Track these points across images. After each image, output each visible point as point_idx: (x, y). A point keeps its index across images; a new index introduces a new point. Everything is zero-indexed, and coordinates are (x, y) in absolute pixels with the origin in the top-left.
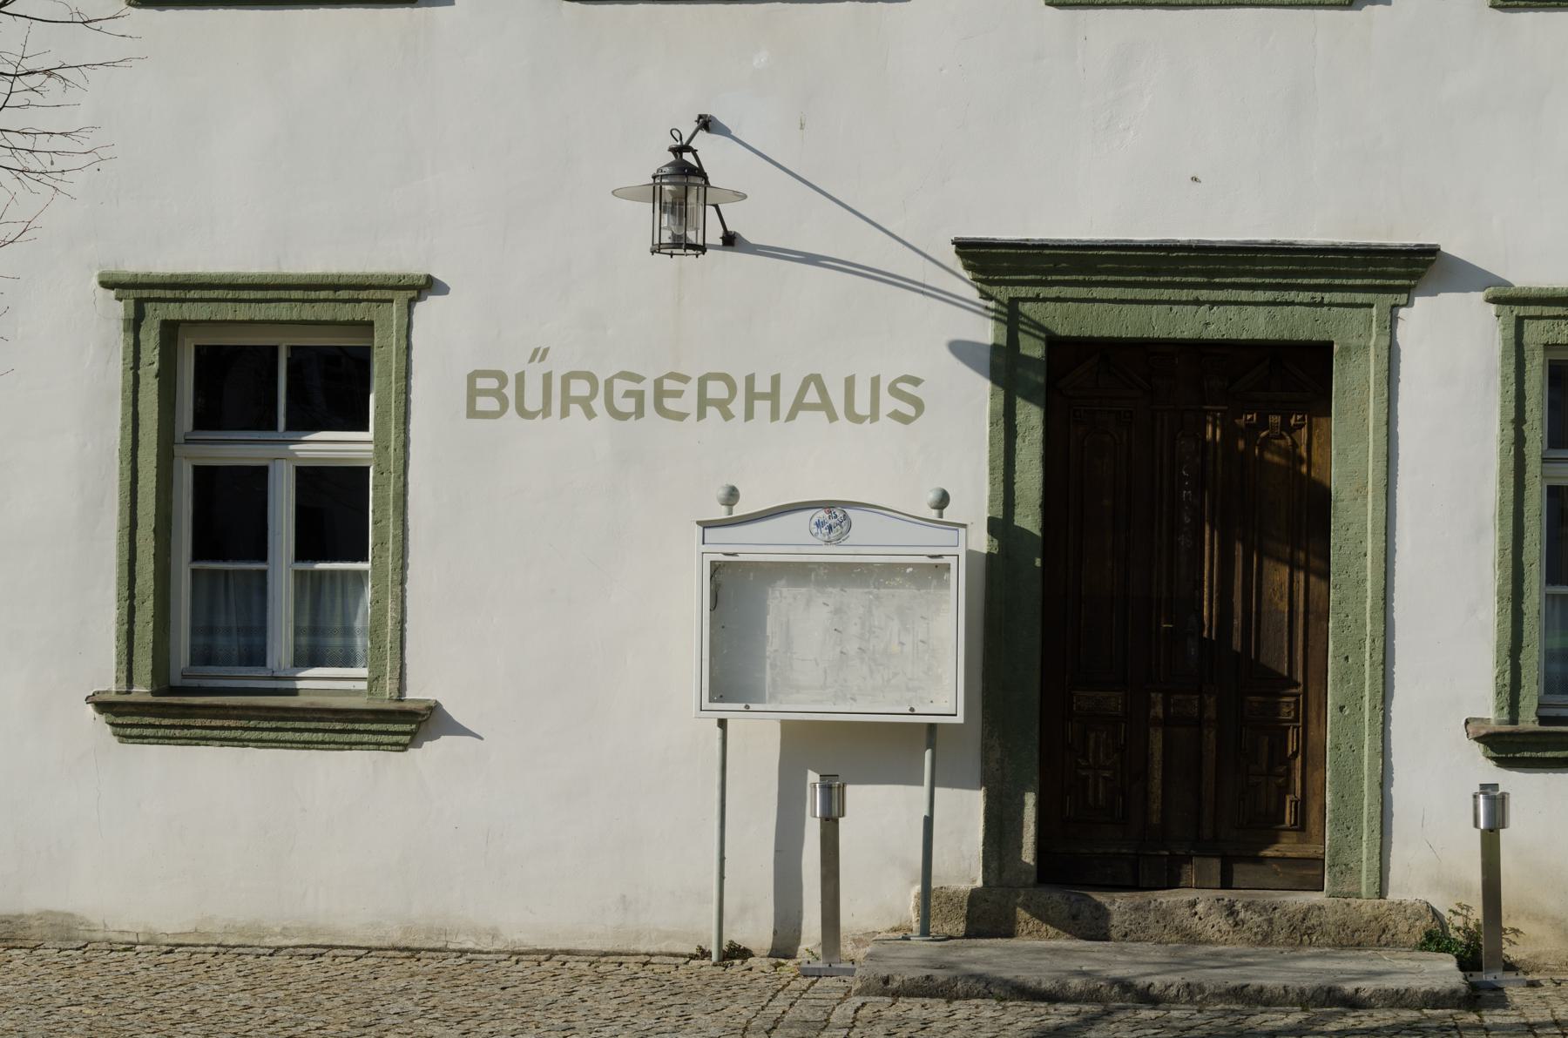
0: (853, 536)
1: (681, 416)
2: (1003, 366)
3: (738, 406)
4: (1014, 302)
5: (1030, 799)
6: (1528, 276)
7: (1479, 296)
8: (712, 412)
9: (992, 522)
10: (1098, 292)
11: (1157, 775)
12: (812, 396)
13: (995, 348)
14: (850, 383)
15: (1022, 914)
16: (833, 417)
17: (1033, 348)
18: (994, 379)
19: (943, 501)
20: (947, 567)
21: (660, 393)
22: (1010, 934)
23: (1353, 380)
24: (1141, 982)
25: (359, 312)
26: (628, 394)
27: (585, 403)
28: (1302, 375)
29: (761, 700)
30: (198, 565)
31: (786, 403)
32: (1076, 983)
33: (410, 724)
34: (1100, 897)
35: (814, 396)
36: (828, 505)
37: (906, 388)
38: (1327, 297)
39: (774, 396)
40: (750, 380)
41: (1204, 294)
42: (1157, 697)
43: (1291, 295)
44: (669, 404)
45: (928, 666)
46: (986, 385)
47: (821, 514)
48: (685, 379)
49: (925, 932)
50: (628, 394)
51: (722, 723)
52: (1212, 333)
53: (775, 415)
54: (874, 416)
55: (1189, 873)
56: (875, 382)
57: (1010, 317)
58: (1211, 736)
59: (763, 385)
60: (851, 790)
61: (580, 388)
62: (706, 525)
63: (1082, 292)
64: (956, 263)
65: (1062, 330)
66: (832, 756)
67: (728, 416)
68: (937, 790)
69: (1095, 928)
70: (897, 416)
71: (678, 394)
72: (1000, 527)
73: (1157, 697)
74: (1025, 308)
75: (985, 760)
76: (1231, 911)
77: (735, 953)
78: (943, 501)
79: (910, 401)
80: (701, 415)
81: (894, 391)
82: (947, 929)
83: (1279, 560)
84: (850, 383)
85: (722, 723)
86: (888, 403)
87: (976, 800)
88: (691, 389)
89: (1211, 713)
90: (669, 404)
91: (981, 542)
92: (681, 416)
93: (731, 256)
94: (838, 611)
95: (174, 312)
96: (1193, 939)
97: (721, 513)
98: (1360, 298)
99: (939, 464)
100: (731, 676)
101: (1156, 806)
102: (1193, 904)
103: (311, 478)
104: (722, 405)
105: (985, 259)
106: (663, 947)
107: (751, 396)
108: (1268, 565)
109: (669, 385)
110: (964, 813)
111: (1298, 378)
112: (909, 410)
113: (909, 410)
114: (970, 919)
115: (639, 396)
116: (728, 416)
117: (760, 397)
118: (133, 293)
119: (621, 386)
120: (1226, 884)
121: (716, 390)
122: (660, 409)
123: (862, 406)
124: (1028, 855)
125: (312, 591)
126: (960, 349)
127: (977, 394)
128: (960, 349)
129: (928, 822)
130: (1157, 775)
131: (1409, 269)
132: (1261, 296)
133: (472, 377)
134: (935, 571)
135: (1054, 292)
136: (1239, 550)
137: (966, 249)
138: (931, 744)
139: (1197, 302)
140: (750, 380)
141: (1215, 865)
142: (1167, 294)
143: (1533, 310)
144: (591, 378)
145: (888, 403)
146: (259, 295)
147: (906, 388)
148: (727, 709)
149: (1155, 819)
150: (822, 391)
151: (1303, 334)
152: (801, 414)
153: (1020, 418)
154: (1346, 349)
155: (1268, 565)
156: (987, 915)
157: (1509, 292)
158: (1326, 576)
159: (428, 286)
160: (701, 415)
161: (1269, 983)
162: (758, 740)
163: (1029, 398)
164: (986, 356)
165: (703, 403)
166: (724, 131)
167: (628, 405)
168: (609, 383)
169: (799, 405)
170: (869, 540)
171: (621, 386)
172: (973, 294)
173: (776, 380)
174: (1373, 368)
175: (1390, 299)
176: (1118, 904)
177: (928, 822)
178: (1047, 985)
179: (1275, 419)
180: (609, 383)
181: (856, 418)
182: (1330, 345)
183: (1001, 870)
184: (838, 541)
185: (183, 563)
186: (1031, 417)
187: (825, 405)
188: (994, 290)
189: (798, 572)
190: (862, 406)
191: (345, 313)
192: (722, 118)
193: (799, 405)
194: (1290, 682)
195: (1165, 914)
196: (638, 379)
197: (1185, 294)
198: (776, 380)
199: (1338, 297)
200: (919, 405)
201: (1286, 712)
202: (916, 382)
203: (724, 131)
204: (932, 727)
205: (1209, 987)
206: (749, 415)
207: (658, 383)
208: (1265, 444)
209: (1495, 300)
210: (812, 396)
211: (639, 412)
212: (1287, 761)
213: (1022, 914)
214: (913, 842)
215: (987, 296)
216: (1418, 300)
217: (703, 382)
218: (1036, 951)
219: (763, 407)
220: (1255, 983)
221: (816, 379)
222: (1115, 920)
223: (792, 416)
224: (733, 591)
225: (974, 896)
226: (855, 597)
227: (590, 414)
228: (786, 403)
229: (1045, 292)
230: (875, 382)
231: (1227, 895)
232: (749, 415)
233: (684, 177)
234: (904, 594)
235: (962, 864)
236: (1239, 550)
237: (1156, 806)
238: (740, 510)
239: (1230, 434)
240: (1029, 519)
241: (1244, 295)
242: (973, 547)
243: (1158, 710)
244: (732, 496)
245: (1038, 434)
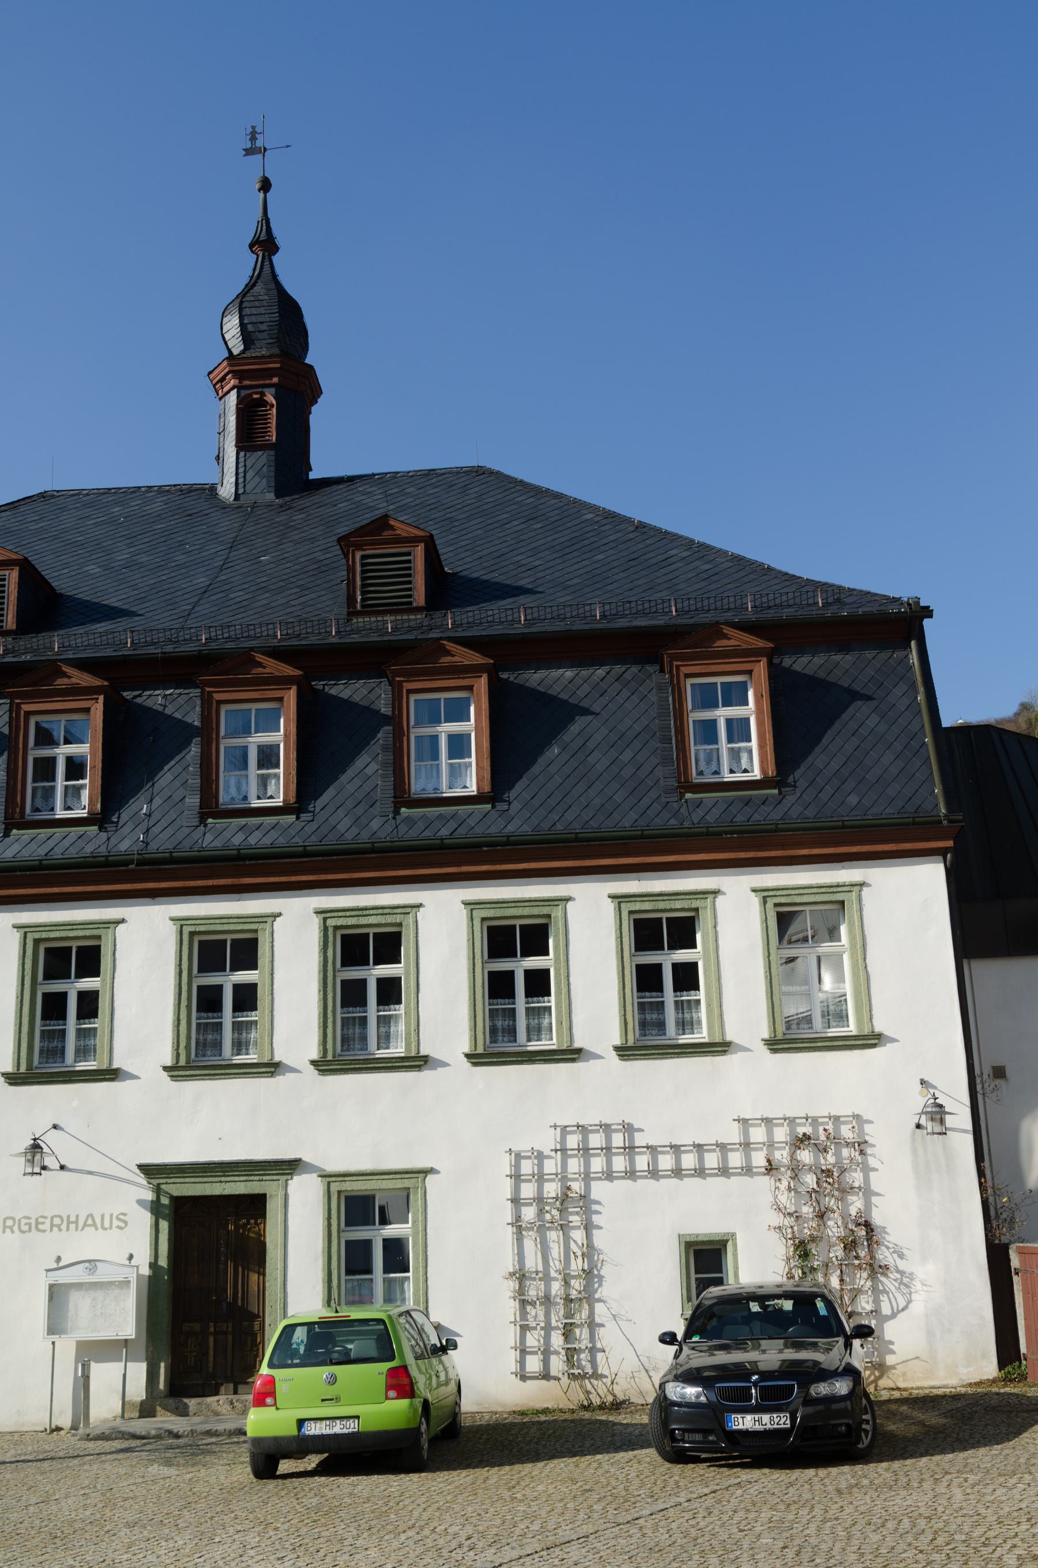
0: (98, 1272)
1: (44, 1231)
2: (155, 1208)
3: (64, 1227)
4: (159, 1184)
5: (162, 1365)
6: (331, 1167)
7: (315, 1175)
8: (55, 1229)
9: (150, 1264)
10: (187, 1180)
11: (211, 1353)
12: (90, 1222)
13: (152, 1201)
14: (103, 1216)
15: (159, 1408)
16: (97, 1229)
17: (165, 1201)
18: (152, 1213)
19: (131, 1257)
20: (129, 1282)
21: (37, 1223)
22: (154, 1416)
23: (273, 1207)
24: (175, 1431)
25: (398, 919)
26: (26, 1224)
27: (59, 1226)
28: (256, 1204)
29: (66, 1333)
30: (386, 1276)
31: (81, 1224)
32: (153, 1432)
33: (111, 1074)
34: (186, 1400)
35: (90, 1223)
36: (89, 1261)
37: (122, 1217)
38: (264, 1178)
39: (76, 1222)
40: (68, 1217)
41: (223, 1179)
42: (211, 1324)
43: (252, 1178)
44: (40, 1227)
45: (123, 1317)
46: (149, 1214)
47: (87, 1264)
48: (46, 1218)
49: (123, 1417)
50: (26, 1224)
51: (53, 1343)
52: (226, 1192)
53: (77, 1229)
54: (111, 1228)
55: (223, 1389)
56: (111, 1215)
57: (158, 1190)
58: (230, 1337)
59: (73, 1219)
60: (93, 1364)
61: (9, 1223)
62: (48, 1271)
63: (182, 1180)
64: (138, 1171)
65: (175, 1194)
66: (91, 1352)
67: (60, 1230)
68: (128, 1364)
69: (183, 1412)
70: (119, 1227)
71: (43, 1223)
72: (154, 1265)
73: (211, 1324)
74: (163, 1187)
75: (147, 1351)
76: (232, 1403)
77: (58, 1429)
78: (131, 1257)
79: (123, 1221)
80: (51, 1230)
81: (118, 1218)
82: (132, 1416)
83: (254, 1272)
84: (103, 1216)
85: (53, 1343)
86: (116, 1223)
87: (143, 1367)
88: (48, 1221)
89: (230, 1329)
90: (40, 1227)
91: (146, 1271)
92: (44, 1231)
93: (62, 1173)
94: (94, 1299)
95: (37, 936)
96: (217, 1414)
97: (55, 1266)
98: (275, 1177)
99: (129, 1244)
100: (55, 1326)
101: (211, 1365)
102: (218, 1401)
103: (529, 974)
104: (59, 1226)
105: (148, 1170)
106: (32, 1429)
107: (69, 1223)
108: (251, 1273)
109: (40, 1220)
110: (138, 1371)
111: (255, 1206)
112: (123, 1225)
113: (123, 1225)
114: (141, 1411)
115: (30, 1225)
116: (60, 1230)
117: (71, 1223)
118: (179, 923)
119: (24, 1221)
120: (235, 1392)
121: (57, 1221)
122: (37, 1229)
123: (107, 1224)
124: (162, 1386)
125: (389, 1284)
126: (141, 1202)
127: (146, 1218)
128: (141, 1202)
129: (125, 1376)
130: (211, 1353)
131: (291, 1167)
132: (242, 1178)
133: (5, 1220)
134: (126, 1283)
135: (172, 1180)
136: (240, 1269)
137: (142, 1167)
138: (126, 1347)
139: (221, 1182)
140: (68, 1217)
141: (231, 1386)
142: (210, 1179)
143: (329, 915)
144: (13, 1219)
145: (116, 1223)
146: (360, 913)
147: (122, 1217)
148: (54, 1338)
149: (211, 1370)
150: (93, 1219)
151: (256, 1192)
152: (86, 1228)
153: (160, 1226)
154: (271, 1196)
155: (251, 1273)
156: (146, 1410)
157: (324, 1173)
158: (264, 1275)
159: (280, 915)
160: (51, 1230)
161: (219, 1428)
162: (67, 1347)
163: (163, 1219)
164: (149, 1204)
165: (52, 1226)
166: (62, 1129)
167: (25, 1228)
168: (20, 1220)
169: (85, 1225)
170: (103, 1274)
171: (24, 1221)
172: (145, 1182)
173: (77, 1216)
174: (280, 1202)
175: (285, 1177)
176: (192, 1403)
177: (125, 1376)
178: (143, 1433)
179: (252, 1221)
180: (20, 1220)
181: (105, 1229)
182: (265, 1195)
183: (152, 1393)
184: (93, 1274)
185: (343, 1277)
186: (164, 1225)
187: (94, 1225)
188: (152, 1181)
189: (79, 1286)
190: (107, 1224)
191: (390, 919)
192: (61, 1125)
193: (85, 1225)
194: (258, 1316)
195: (208, 1406)
196: (29, 1218)
197: (216, 1179)
198: (77, 1216)
199: (268, 1178)
200: (126, 1223)
201: (256, 1327)
202: (125, 1215)
203: (62, 1129)
204: (126, 1340)
205: (199, 1430)
206: (68, 1229)
207: (37, 1219)
208: (249, 1230)
209: (320, 1176)
210: (90, 1222)
211: (30, 1230)
212: (257, 1346)
213: (159, 1408)
214: (120, 1385)
215: (149, 1183)
216: (295, 1178)
217: (52, 1219)
218: (165, 1420)
219: (72, 1226)
220: (215, 1429)
221: (91, 1215)
222: (191, 1409)
223: (83, 1229)
224: (56, 1294)
225: (142, 1403)
226: (99, 1294)
227: (13, 1232)
228: (81, 1224)
229: (169, 1181)
230: (111, 1215)
231: (236, 1397)
232: (68, 1229)
233: (36, 1147)
234: (117, 1291)
235: (138, 1390)
236: (240, 1269)
237: (211, 1365)
238: (61, 1264)
239: (237, 1227)
240: (163, 1262)
241: (236, 1179)
242: (141, 1272)
243: (212, 1329)
244: (59, 1259)
245: (166, 1231)
